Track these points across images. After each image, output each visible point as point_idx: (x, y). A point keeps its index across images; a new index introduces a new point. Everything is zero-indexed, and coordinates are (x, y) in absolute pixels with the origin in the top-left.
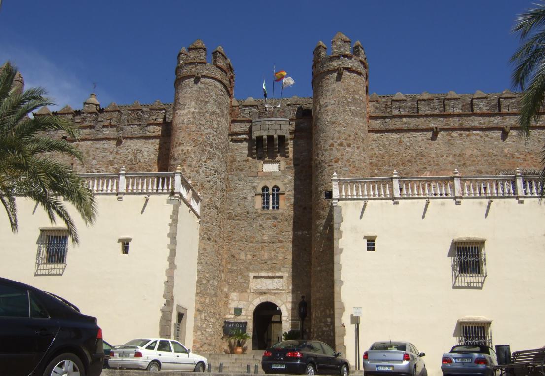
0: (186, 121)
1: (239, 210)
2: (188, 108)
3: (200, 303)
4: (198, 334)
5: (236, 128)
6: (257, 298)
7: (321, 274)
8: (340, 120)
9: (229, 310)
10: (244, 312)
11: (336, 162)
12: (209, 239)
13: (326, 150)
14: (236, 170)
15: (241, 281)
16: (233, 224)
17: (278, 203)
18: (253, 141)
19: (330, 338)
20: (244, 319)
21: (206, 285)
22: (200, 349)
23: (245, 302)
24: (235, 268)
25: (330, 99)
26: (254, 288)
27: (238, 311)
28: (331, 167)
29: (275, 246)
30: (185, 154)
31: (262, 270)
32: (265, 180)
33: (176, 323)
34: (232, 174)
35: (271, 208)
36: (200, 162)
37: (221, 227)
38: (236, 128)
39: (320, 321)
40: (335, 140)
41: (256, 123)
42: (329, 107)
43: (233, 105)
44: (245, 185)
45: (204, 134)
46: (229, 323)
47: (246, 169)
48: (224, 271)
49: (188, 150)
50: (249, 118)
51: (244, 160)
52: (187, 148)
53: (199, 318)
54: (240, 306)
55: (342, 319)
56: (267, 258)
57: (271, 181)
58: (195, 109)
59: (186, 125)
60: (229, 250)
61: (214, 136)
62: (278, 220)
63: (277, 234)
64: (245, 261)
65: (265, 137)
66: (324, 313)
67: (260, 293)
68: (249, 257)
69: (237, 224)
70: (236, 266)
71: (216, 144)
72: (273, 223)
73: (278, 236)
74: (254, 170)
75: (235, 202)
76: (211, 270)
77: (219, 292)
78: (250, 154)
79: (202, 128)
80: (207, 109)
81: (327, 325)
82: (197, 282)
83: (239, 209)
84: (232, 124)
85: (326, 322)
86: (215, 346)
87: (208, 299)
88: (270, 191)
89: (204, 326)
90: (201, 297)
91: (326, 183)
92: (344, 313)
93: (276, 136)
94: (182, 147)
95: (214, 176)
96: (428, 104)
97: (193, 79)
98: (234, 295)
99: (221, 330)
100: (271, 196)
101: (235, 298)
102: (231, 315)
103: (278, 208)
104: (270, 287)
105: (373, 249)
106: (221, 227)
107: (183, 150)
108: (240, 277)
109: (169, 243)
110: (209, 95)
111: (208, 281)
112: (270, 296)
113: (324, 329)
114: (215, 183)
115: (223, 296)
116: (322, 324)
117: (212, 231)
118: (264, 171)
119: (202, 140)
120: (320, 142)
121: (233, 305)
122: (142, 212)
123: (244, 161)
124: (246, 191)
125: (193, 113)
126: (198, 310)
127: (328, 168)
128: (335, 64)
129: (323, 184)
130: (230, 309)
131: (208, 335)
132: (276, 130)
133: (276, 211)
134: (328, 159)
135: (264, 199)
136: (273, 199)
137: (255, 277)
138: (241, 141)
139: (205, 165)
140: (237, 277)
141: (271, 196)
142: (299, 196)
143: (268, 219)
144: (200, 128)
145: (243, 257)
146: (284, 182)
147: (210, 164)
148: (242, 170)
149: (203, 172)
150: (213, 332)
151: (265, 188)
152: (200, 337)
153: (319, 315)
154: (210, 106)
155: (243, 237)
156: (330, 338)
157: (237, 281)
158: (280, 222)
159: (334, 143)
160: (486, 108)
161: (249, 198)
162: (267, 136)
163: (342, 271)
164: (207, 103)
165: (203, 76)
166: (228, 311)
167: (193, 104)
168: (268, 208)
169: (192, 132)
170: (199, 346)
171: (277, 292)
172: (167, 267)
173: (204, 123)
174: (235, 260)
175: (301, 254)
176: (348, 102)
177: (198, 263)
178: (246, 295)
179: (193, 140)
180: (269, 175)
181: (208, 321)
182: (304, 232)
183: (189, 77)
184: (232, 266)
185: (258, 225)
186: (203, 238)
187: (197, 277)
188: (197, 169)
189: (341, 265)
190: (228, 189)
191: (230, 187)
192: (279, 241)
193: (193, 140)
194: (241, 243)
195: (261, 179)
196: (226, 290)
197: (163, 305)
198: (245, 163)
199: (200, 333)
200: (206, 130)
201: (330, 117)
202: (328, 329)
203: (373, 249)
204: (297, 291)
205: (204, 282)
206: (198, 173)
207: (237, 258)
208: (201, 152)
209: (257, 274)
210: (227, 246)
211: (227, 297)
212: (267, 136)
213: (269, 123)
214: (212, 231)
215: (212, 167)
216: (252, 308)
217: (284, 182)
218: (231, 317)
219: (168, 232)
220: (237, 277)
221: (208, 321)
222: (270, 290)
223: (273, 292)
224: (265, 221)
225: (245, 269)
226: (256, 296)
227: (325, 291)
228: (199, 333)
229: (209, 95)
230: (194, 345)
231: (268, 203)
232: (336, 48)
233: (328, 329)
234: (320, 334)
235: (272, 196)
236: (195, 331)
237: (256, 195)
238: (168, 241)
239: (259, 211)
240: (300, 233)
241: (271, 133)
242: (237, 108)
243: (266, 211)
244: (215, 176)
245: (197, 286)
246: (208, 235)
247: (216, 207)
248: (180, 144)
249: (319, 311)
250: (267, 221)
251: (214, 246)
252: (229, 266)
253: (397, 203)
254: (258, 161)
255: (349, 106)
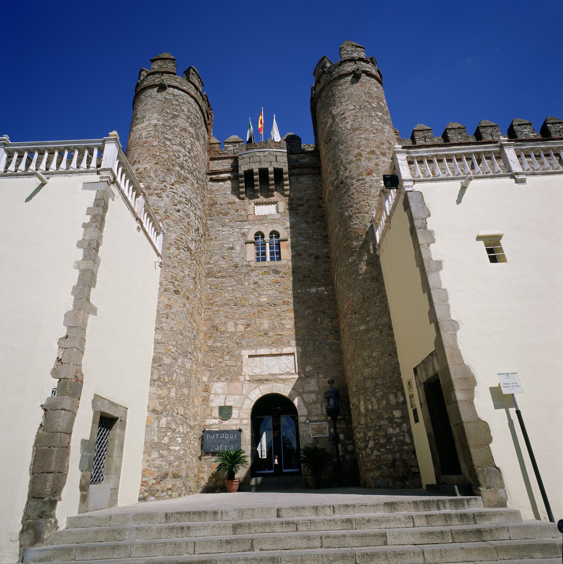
0: (143, 135)
1: (223, 264)
2: (148, 120)
3: (159, 397)
4: (153, 456)
5: (216, 166)
6: (255, 388)
7: (369, 336)
8: (366, 125)
9: (211, 411)
10: (235, 413)
11: (369, 174)
12: (177, 292)
13: (350, 163)
14: (218, 215)
15: (229, 363)
16: (214, 283)
17: (279, 253)
18: (241, 176)
19: (406, 448)
20: (236, 425)
21: (171, 365)
22: (158, 487)
23: (236, 397)
24: (219, 344)
25: (347, 105)
26: (251, 374)
27: (225, 412)
28: (361, 182)
29: (278, 310)
30: (140, 173)
31: (261, 346)
32: (258, 224)
33: (87, 437)
34: (211, 220)
35: (268, 259)
36: (164, 184)
37: (196, 280)
38: (216, 166)
39: (380, 418)
40: (362, 148)
41: (244, 156)
42: (348, 114)
43: (211, 142)
44: (231, 232)
45: (171, 150)
46: (211, 433)
47: (232, 213)
48: (203, 350)
49: (145, 169)
50: (232, 155)
51: (228, 202)
52: (144, 166)
53: (155, 425)
54: (228, 404)
55: (475, 401)
56: (267, 328)
57: (267, 225)
58: (158, 121)
59: (144, 140)
60: (210, 319)
61: (186, 156)
62: (281, 275)
63: (280, 292)
64: (234, 333)
65: (256, 170)
66: (384, 402)
67: (260, 381)
68: (241, 328)
69: (221, 283)
70: (220, 342)
71: (188, 167)
72: (273, 278)
73: (282, 295)
74: (243, 213)
75: (216, 255)
76: (179, 342)
77: (193, 381)
78: (235, 191)
79: (168, 143)
80: (177, 124)
81: (396, 423)
82: (154, 360)
83: (224, 263)
84: (211, 162)
85: (391, 420)
86: (187, 476)
87: (173, 390)
88: (267, 238)
89: (166, 440)
90: (159, 386)
91: (356, 204)
92: (476, 389)
93: (271, 169)
94: (137, 166)
95: (185, 205)
96: (459, 133)
97: (156, 89)
98: (218, 387)
99: (197, 444)
100: (268, 244)
101: (220, 391)
102: (215, 418)
103: (279, 259)
104: (276, 371)
105: (503, 259)
106: (196, 280)
107: (137, 170)
108: (227, 358)
109: (81, 258)
110: (178, 108)
111: (174, 359)
112: (276, 384)
113: (390, 431)
114: (188, 216)
115: (200, 389)
116: (383, 422)
117: (182, 282)
118: (256, 214)
119: (167, 156)
120: (340, 156)
121: (217, 402)
122: (28, 199)
123: (228, 203)
124: (232, 240)
125: (156, 125)
126: (154, 411)
127: (356, 184)
128: (349, 67)
129: (351, 206)
130: (212, 409)
131: (172, 458)
132: (271, 162)
133: (276, 263)
134: (355, 173)
135: (258, 249)
136: (271, 248)
137: (250, 356)
138: (223, 180)
139: (171, 188)
140: (223, 358)
141: (268, 244)
142: (308, 242)
143: (265, 273)
144: (164, 143)
145: (231, 327)
146: (284, 226)
147: (180, 189)
148: (225, 214)
149: (168, 196)
150: (182, 452)
151: (259, 235)
152: (158, 462)
153: (376, 407)
154: (179, 121)
155: (230, 300)
156: (406, 448)
157: (224, 364)
158: (284, 277)
159: (363, 152)
160: (533, 134)
161: (238, 248)
162: (259, 169)
163: (451, 302)
164: (175, 117)
165: (170, 86)
166: (209, 412)
167: (156, 115)
168: (264, 260)
169: (153, 146)
170: (154, 481)
171: (287, 377)
172: (71, 308)
173: (171, 137)
174: (219, 334)
175: (319, 319)
176: (373, 107)
177: (157, 329)
178: (237, 384)
179: (154, 156)
180: (263, 219)
181: (174, 431)
182: (320, 288)
183: (151, 87)
184: (215, 342)
185: (252, 281)
186: (166, 290)
187: (154, 352)
188: (159, 192)
189: (445, 290)
190: (205, 235)
191: (209, 236)
192: (284, 302)
193: (154, 156)
194: (227, 308)
195: (254, 224)
196: (205, 379)
197: (49, 394)
198: (229, 206)
199: (157, 455)
200: (174, 146)
201: (350, 124)
202: (397, 430)
203: (503, 259)
204: (318, 373)
205: (167, 361)
206: (160, 197)
207: (222, 330)
208: (165, 171)
209: (254, 351)
210: (206, 313)
211: (207, 389)
212: (259, 169)
213: (261, 154)
214: (182, 282)
215: (182, 193)
216: (249, 405)
217: (284, 226)
218: (214, 423)
219: (81, 238)
220: (223, 358)
221: (174, 431)
222: (275, 375)
223: (281, 377)
224: (261, 277)
225: (235, 345)
226: (253, 385)
227: (381, 362)
228: (155, 455)
229: (178, 108)
230: (145, 479)
231: (264, 254)
232: (347, 54)
233: (397, 430)
234: (382, 441)
235: (270, 245)
236: (147, 452)
237: (246, 243)
238: (79, 254)
239: (253, 264)
240: (314, 290)
241: (264, 166)
242: (217, 146)
243: (262, 264)
244: (187, 207)
245: (153, 367)
246: (175, 287)
247: (189, 250)
248: (135, 162)
249: (374, 400)
250: (264, 276)
251: (185, 305)
252: (210, 343)
253: (523, 181)
254: (247, 200)
255: (375, 111)
